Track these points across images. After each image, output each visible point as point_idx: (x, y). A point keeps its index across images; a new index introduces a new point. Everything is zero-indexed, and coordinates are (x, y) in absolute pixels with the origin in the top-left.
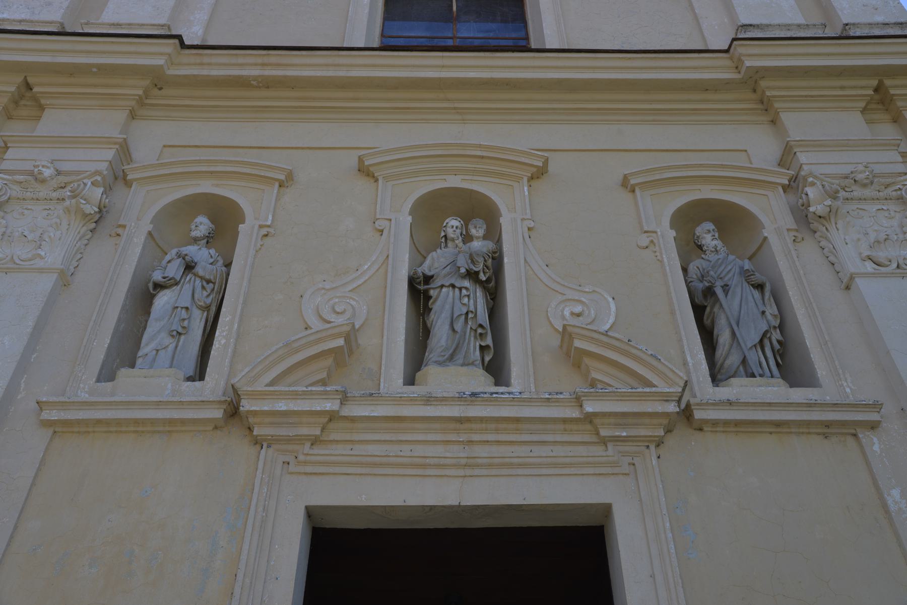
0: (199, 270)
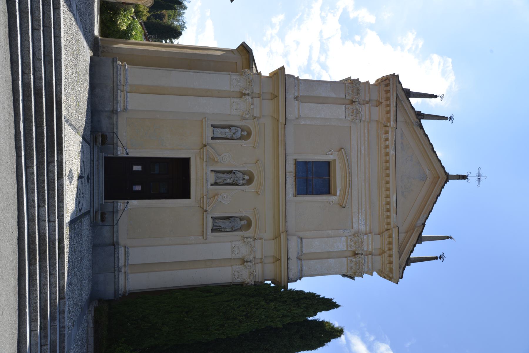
0: (234, 135)
